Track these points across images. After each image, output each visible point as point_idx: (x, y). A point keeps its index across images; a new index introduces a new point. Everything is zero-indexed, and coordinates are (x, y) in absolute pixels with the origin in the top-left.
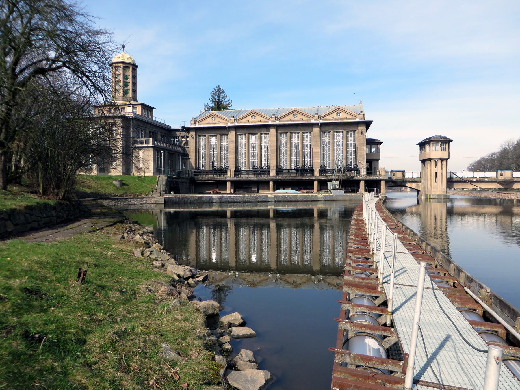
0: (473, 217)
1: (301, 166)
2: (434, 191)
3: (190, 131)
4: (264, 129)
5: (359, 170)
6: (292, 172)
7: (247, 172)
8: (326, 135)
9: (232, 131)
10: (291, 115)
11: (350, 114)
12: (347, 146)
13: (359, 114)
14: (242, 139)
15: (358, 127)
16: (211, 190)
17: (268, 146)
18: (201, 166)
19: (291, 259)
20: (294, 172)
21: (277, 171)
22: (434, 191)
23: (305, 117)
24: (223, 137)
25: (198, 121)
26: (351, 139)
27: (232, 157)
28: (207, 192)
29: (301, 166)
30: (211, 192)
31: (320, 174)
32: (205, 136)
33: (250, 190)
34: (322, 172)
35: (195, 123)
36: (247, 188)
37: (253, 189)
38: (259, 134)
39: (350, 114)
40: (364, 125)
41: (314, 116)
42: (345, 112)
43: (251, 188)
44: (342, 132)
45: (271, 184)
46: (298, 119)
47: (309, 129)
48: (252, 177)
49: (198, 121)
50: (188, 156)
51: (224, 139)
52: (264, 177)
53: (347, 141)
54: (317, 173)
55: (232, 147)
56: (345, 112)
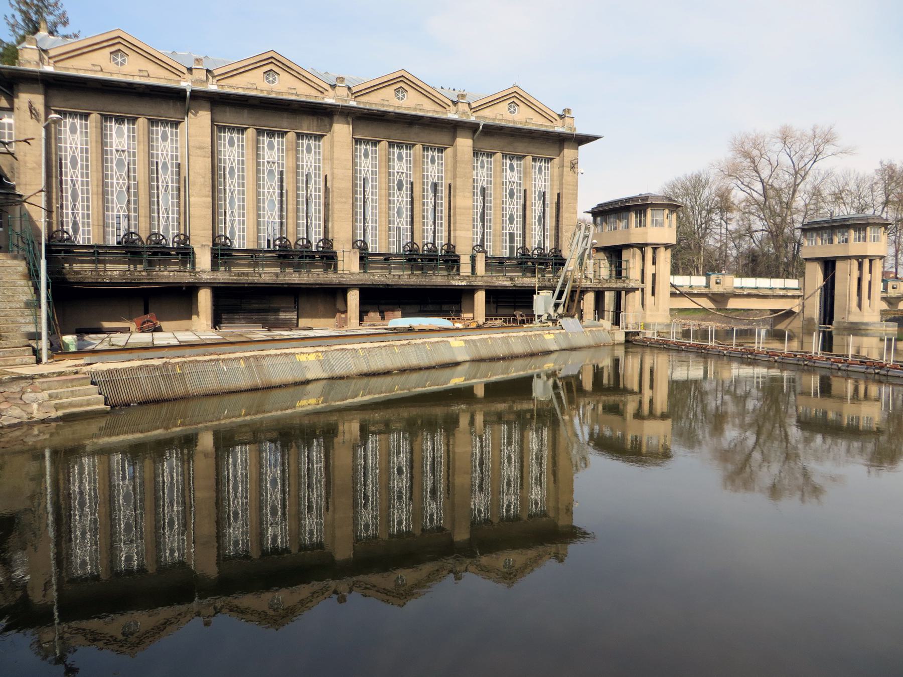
0: (688, 366)
1: (144, 236)
2: (651, 316)
3: (21, 87)
4: (310, 118)
5: (193, 253)
6: (240, 258)
7: (254, 256)
8: (482, 161)
9: (201, 113)
10: (390, 91)
11: (541, 113)
12: (150, 172)
13: (455, 103)
14: (73, 130)
15: (561, 150)
16: (130, 319)
17: (281, 173)
18: (69, 228)
19: (387, 520)
20: (400, 263)
21: (215, 256)
22: (651, 316)
23: (429, 101)
24: (227, 135)
25: (52, 53)
26: (308, 161)
27: (200, 202)
28: (107, 325)
29: (144, 236)
30: (133, 326)
31: (212, 265)
32: (86, 116)
33: (271, 317)
34: (155, 258)
35: (41, 59)
36: (259, 311)
37: (282, 315)
38: (291, 135)
39: (541, 113)
40: (41, 87)
41: (333, 87)
42: (530, 105)
43: (277, 311)
44: (283, 134)
45: (205, 298)
46: (522, 118)
47: (441, 138)
48: (267, 275)
49: (52, 53)
50: (13, 188)
51: (165, 138)
52: (169, 274)
53: (150, 155)
54: (204, 260)
55: (200, 167)
56: (530, 105)
